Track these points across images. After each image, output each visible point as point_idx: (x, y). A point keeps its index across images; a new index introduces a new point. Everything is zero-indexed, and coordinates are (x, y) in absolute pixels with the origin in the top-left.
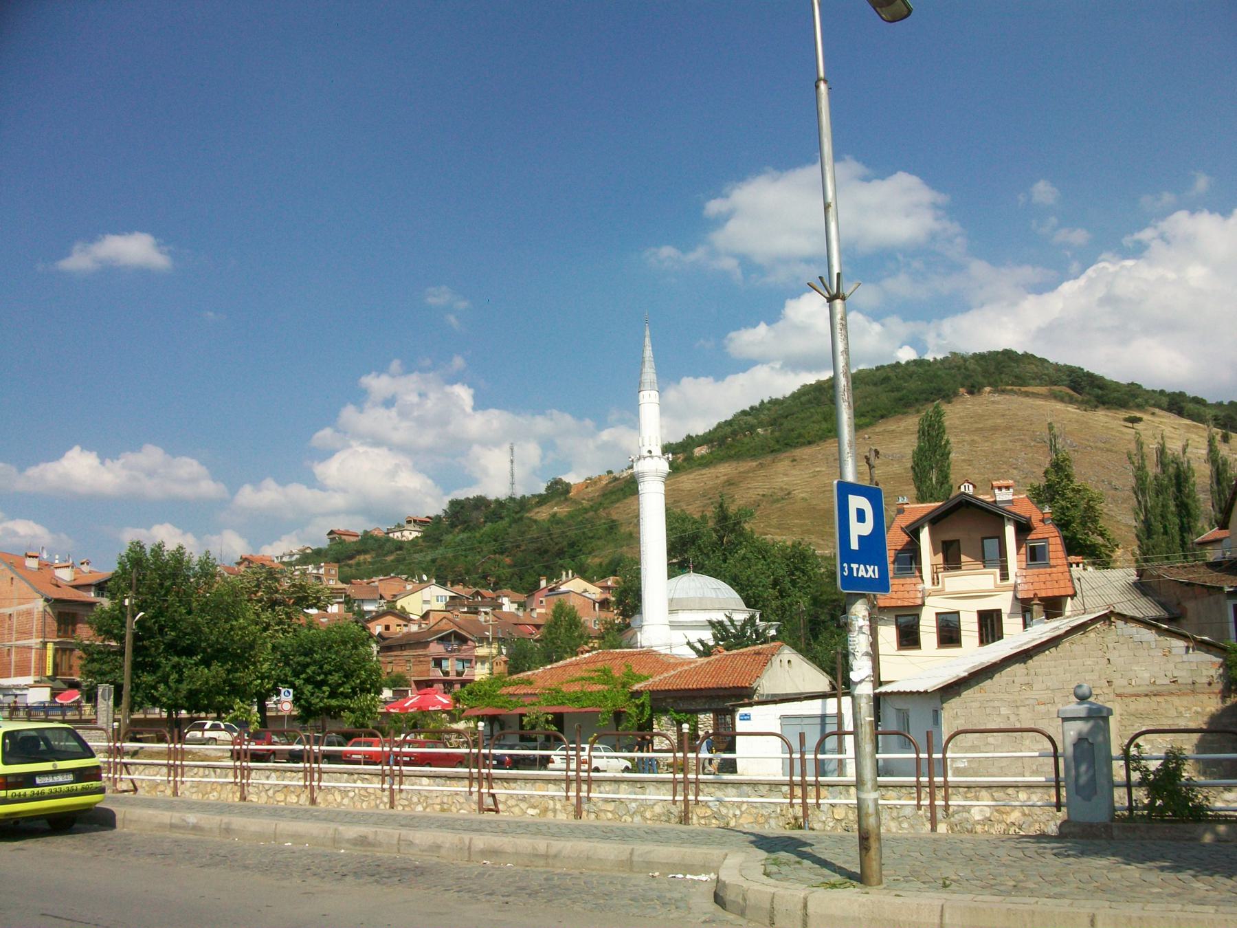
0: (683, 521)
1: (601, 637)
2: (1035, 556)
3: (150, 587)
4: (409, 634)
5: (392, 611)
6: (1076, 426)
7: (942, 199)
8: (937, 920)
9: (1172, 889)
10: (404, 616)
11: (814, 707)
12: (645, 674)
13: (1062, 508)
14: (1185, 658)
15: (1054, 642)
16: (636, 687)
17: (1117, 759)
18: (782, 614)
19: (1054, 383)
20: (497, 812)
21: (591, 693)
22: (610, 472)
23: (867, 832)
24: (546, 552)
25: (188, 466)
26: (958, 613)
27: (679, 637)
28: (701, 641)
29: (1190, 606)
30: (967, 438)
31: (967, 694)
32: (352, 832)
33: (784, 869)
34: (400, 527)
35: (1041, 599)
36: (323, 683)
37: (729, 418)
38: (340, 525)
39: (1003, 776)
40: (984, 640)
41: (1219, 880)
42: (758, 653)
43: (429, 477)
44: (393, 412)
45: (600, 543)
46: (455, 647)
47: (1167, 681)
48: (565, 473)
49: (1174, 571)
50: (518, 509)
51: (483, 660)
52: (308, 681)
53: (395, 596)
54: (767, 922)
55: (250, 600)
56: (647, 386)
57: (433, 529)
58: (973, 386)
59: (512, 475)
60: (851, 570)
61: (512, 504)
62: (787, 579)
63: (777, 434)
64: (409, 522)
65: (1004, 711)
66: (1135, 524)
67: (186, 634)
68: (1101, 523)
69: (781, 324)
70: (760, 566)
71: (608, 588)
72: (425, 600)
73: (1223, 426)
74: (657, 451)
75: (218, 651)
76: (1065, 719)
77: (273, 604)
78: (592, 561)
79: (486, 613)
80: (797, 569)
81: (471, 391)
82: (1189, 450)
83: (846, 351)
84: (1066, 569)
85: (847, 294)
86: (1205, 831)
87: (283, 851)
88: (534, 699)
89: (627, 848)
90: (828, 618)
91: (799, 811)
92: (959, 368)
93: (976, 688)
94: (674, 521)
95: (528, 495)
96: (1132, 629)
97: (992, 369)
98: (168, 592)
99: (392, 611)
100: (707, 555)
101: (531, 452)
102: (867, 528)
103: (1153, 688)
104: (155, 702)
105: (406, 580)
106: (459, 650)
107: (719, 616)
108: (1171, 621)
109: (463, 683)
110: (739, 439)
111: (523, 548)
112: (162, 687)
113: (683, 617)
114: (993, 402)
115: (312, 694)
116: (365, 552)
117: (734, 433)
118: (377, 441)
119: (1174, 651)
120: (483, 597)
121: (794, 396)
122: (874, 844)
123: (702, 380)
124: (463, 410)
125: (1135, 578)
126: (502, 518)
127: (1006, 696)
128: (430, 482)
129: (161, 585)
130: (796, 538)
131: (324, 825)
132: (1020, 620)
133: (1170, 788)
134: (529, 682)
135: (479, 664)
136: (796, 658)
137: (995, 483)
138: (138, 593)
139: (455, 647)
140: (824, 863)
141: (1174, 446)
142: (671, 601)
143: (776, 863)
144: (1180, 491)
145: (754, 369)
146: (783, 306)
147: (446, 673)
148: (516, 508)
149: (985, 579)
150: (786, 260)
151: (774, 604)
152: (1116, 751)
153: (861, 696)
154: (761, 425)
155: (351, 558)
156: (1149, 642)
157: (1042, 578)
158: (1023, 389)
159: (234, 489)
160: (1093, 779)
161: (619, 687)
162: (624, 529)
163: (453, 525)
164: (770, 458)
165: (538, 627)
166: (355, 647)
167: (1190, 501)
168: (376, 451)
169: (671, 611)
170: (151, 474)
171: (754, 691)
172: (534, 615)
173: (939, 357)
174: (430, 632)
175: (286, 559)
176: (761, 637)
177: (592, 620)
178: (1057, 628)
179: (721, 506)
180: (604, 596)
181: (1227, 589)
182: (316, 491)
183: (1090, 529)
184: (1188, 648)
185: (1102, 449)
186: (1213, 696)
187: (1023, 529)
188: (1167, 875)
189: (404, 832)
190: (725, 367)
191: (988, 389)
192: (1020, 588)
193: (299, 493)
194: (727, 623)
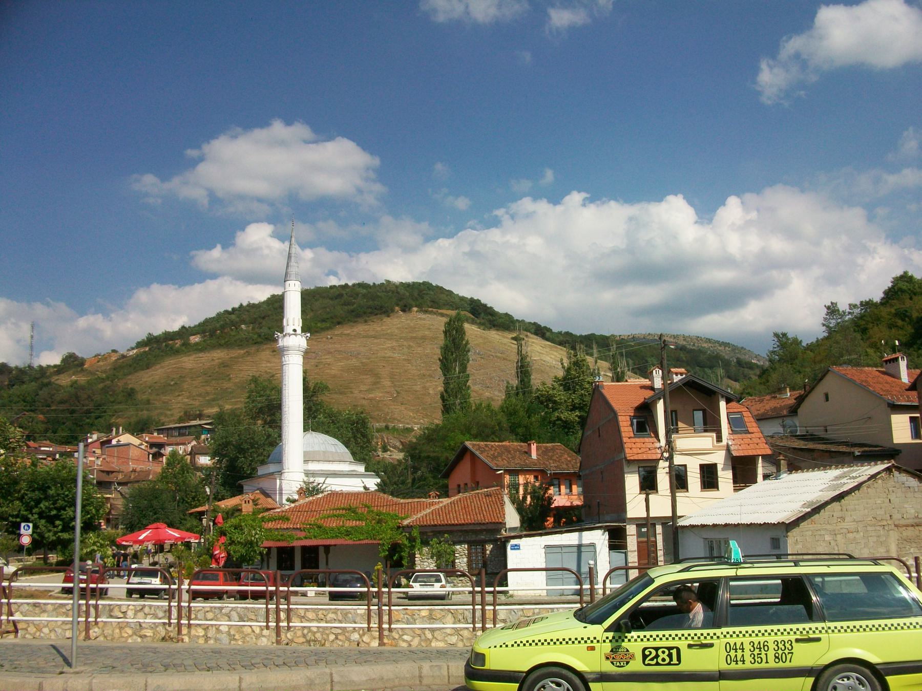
6: (481, 341)
13: (582, 395)
30: (405, 343)
36: (57, 517)
45: (121, 407)
56: (293, 277)
65: (827, 538)
92: (393, 292)
103: (916, 521)
114: (420, 319)
117: (223, 327)
127: (829, 527)
146: (234, 237)
149: (706, 441)
150: (242, 197)
154: (243, 322)
157: (746, 441)
158: (440, 311)
164: (253, 349)
169: (306, 461)
185: (499, 358)
191: (415, 309)
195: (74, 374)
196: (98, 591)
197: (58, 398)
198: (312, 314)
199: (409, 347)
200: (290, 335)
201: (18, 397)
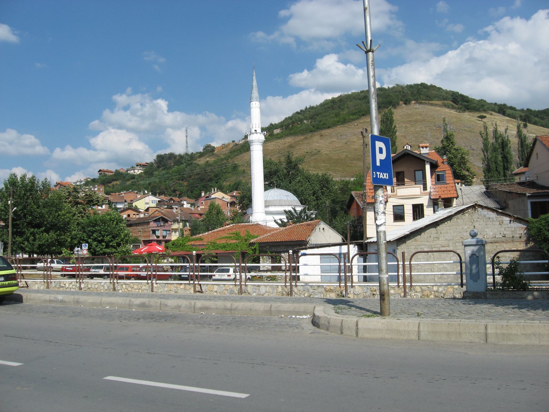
0: (271, 163)
1: (233, 219)
2: (439, 179)
3: (19, 196)
4: (139, 218)
5: (130, 208)
6: (455, 120)
7: (395, 8)
8: (417, 329)
9: (519, 315)
10: (136, 210)
11: (335, 250)
12: (256, 234)
14: (509, 225)
15: (449, 218)
16: (252, 241)
17: (489, 264)
18: (317, 207)
19: (445, 99)
20: (202, 292)
21: (230, 244)
22: (233, 141)
23: (384, 292)
24: (204, 179)
25: (29, 139)
26: (403, 205)
27: (270, 217)
28: (281, 220)
29: (510, 203)
30: (404, 125)
31: (409, 242)
32: (138, 301)
33: (344, 311)
34: (133, 168)
35: (442, 199)
36: (102, 241)
37: (290, 115)
38: (104, 167)
39: (437, 271)
40: (415, 218)
41: (540, 311)
42: (309, 225)
43: (146, 144)
44: (128, 113)
45: (230, 175)
46: (162, 224)
47: (501, 236)
48: (212, 142)
49: (503, 186)
50: (190, 159)
51: (175, 230)
52: (95, 240)
53: (132, 201)
54: (339, 332)
55: (66, 202)
56: (254, 99)
57: (149, 169)
58: (406, 101)
59: (187, 143)
60: (377, 175)
61: (187, 157)
62: (320, 191)
63: (313, 123)
64: (137, 165)
66: (482, 165)
67: (36, 218)
68: (468, 165)
69: (314, 71)
70: (306, 185)
71: (234, 196)
72: (146, 202)
73: (524, 120)
74: (259, 130)
75: (53, 225)
76: (465, 246)
77: (77, 203)
78: (226, 184)
79: (176, 208)
80: (324, 187)
81: (167, 103)
82: (508, 131)
83: (374, 76)
84: (454, 185)
85: (374, 49)
86: (528, 295)
87: (106, 310)
88: (204, 247)
89: (268, 305)
90: (340, 209)
91: (343, 289)
92: (400, 92)
93: (413, 239)
94: (267, 164)
95: (194, 152)
96: (485, 212)
97: (415, 92)
98: (28, 198)
99: (130, 208)
100: (282, 180)
101: (195, 132)
102: (383, 156)
103: (494, 239)
104: (24, 251)
105: (137, 193)
106: (164, 226)
107: (289, 208)
108: (502, 209)
109: (167, 241)
110: (293, 126)
111: (193, 177)
112: (26, 243)
113: (272, 209)
114: (416, 108)
115: (97, 246)
116: (116, 180)
117: (293, 123)
118: (120, 127)
119: (504, 222)
120: (174, 201)
121: (322, 105)
122: (386, 297)
123: (277, 98)
124: (163, 112)
125: (485, 190)
126: (182, 163)
127: (427, 243)
128: (147, 146)
129: (25, 194)
130: (324, 172)
131: (124, 298)
132: (432, 209)
133: (512, 276)
134: (201, 239)
135: (173, 232)
136: (327, 227)
137: (420, 145)
138: (13, 197)
139: (162, 224)
140: (361, 309)
141: (501, 130)
142: (266, 201)
143: (339, 308)
144: (503, 150)
145: (302, 92)
146: (315, 62)
147: (158, 237)
148: (187, 159)
149: (417, 190)
150: (317, 39)
151: (314, 203)
152: (488, 259)
153: (381, 231)
154: (306, 118)
155: (110, 182)
156: (493, 218)
157: (443, 189)
158: (430, 102)
159: (52, 150)
160: (478, 272)
161: (244, 241)
162: (241, 169)
163: (158, 167)
164: (310, 135)
165: (201, 215)
166: (117, 224)
167: (508, 155)
168: (120, 131)
169: (266, 206)
170: (11, 143)
171: (308, 242)
172: (199, 209)
173: (391, 86)
174: (150, 217)
175: (78, 184)
176: (309, 218)
177: (227, 212)
178: (451, 212)
179: (288, 157)
180: (232, 200)
181: (528, 194)
182: (91, 151)
183: (462, 167)
184: (511, 221)
185: (466, 131)
186: (521, 243)
187: (434, 166)
188: (516, 310)
189: (163, 301)
190: (288, 90)
191: (413, 102)
192: (432, 194)
193: (83, 152)
194: (293, 211)
195: (208, 157)
196: (114, 276)
197: (195, 172)
198: (347, 110)
199: (406, 127)
200: (253, 134)
201: (176, 172)
